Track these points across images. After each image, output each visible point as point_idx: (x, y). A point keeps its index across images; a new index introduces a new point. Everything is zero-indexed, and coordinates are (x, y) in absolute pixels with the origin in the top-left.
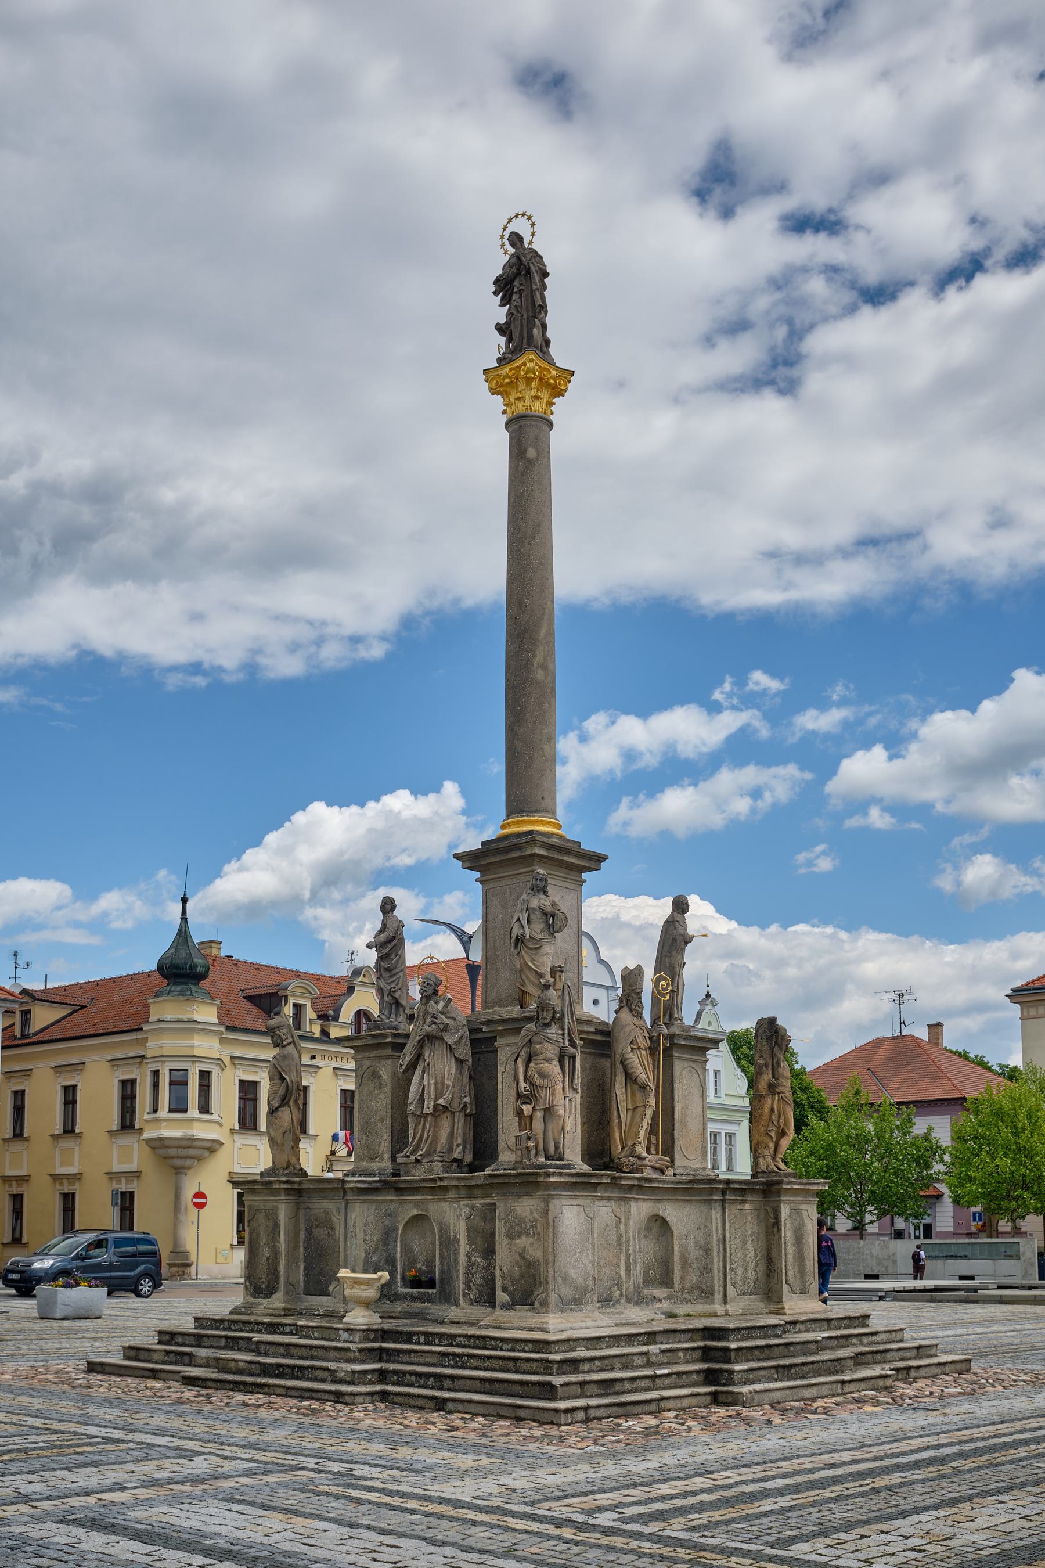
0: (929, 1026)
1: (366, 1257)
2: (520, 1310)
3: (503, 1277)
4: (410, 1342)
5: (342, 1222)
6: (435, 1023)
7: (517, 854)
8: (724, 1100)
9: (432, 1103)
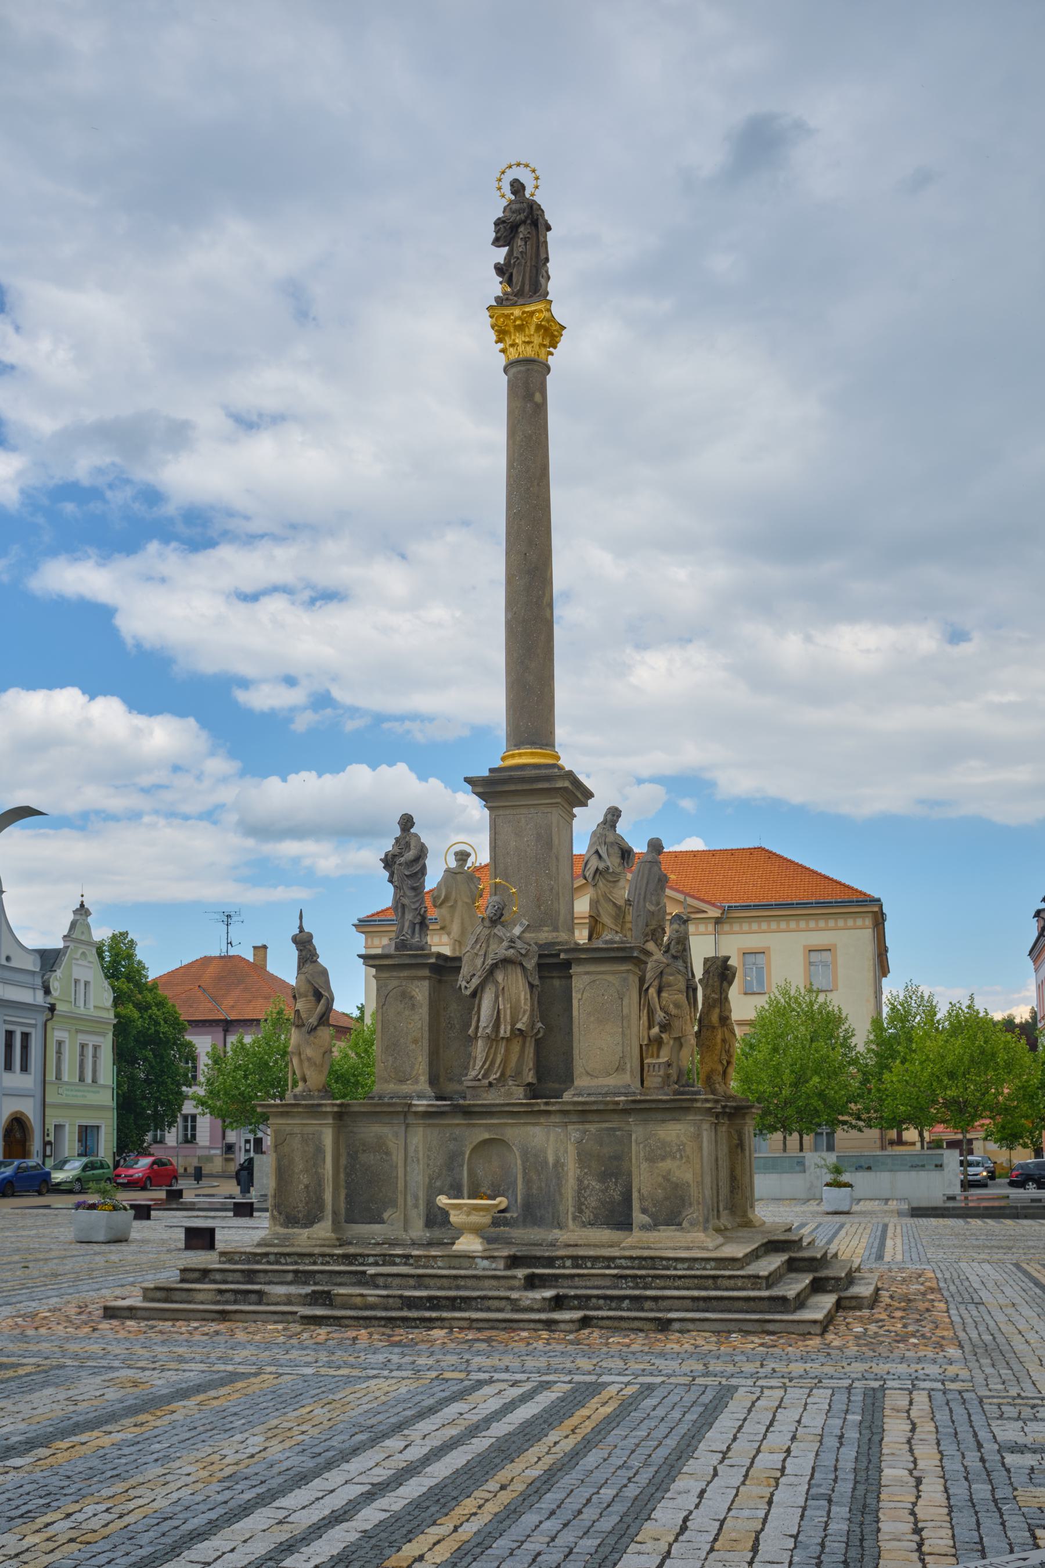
0: (255, 948)
1: (430, 1182)
2: (664, 1231)
3: (642, 1199)
4: (553, 1267)
5: (402, 1147)
6: (512, 947)
7: (546, 785)
8: (92, 1012)
9: (509, 1028)
